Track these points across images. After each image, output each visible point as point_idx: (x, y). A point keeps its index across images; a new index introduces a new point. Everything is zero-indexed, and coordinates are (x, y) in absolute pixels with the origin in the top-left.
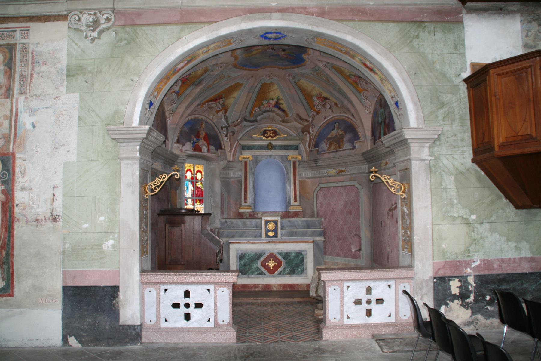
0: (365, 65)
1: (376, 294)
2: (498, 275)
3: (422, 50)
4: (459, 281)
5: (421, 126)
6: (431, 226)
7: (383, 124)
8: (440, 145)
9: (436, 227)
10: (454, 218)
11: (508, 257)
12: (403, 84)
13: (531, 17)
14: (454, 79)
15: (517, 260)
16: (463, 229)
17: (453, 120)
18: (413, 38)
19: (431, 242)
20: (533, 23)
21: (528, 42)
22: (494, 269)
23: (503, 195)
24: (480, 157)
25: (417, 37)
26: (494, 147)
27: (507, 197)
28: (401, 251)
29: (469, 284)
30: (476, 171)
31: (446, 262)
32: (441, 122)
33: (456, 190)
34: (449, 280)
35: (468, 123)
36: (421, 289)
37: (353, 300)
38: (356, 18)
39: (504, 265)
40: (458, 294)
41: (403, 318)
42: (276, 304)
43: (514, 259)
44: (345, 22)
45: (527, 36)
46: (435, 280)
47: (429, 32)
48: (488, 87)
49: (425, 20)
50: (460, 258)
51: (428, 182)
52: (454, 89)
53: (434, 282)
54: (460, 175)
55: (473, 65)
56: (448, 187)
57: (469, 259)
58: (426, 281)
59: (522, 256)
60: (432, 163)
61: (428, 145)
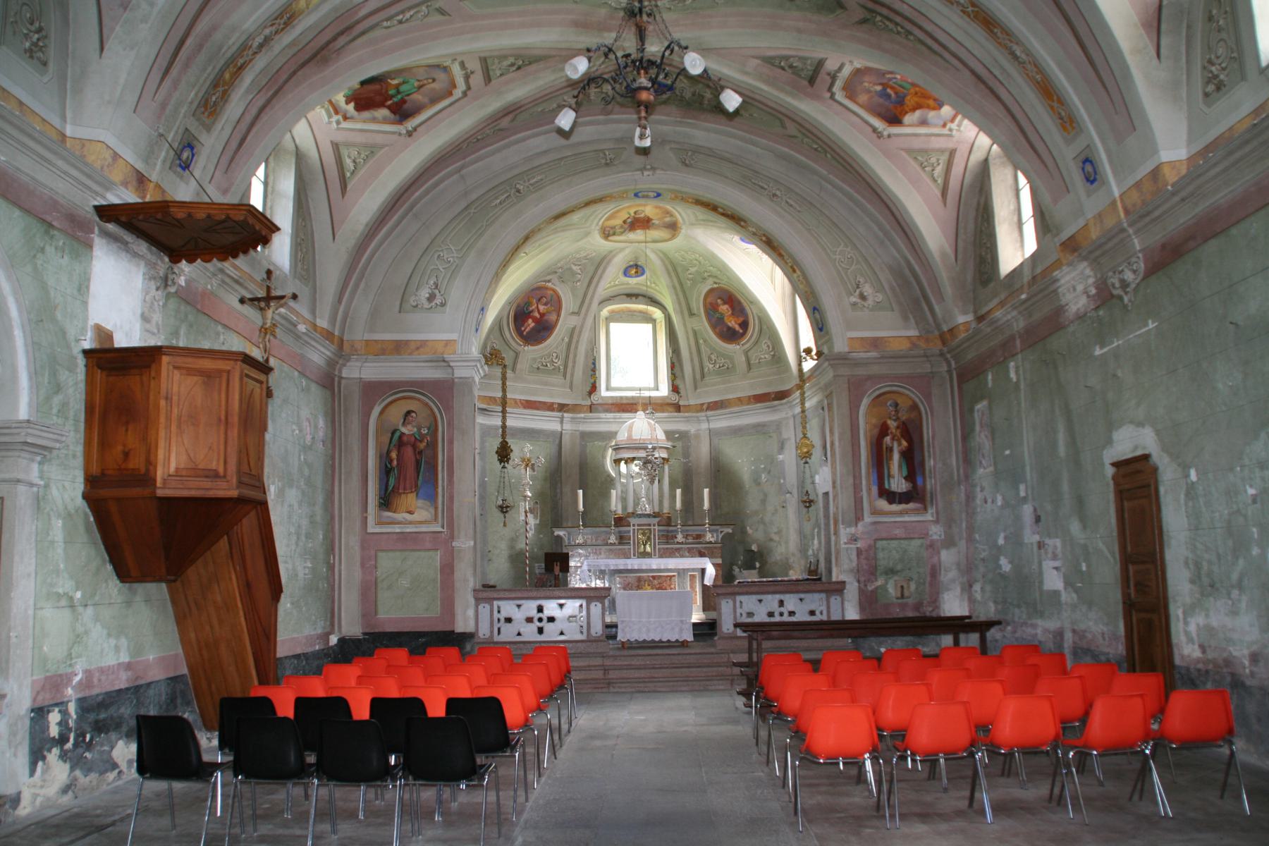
9: (39, 612)
11: (107, 664)
12: (21, 334)
15: (116, 667)
16: (67, 613)
20: (153, 282)
23: (107, 558)
26: (155, 480)
30: (86, 514)
40: (57, 737)
43: (113, 666)
45: (145, 301)
46: (32, 715)
47: (56, 248)
49: (55, 223)
51: (34, 527)
53: (32, 719)
54: (68, 517)
57: (70, 670)
61: (39, 458)
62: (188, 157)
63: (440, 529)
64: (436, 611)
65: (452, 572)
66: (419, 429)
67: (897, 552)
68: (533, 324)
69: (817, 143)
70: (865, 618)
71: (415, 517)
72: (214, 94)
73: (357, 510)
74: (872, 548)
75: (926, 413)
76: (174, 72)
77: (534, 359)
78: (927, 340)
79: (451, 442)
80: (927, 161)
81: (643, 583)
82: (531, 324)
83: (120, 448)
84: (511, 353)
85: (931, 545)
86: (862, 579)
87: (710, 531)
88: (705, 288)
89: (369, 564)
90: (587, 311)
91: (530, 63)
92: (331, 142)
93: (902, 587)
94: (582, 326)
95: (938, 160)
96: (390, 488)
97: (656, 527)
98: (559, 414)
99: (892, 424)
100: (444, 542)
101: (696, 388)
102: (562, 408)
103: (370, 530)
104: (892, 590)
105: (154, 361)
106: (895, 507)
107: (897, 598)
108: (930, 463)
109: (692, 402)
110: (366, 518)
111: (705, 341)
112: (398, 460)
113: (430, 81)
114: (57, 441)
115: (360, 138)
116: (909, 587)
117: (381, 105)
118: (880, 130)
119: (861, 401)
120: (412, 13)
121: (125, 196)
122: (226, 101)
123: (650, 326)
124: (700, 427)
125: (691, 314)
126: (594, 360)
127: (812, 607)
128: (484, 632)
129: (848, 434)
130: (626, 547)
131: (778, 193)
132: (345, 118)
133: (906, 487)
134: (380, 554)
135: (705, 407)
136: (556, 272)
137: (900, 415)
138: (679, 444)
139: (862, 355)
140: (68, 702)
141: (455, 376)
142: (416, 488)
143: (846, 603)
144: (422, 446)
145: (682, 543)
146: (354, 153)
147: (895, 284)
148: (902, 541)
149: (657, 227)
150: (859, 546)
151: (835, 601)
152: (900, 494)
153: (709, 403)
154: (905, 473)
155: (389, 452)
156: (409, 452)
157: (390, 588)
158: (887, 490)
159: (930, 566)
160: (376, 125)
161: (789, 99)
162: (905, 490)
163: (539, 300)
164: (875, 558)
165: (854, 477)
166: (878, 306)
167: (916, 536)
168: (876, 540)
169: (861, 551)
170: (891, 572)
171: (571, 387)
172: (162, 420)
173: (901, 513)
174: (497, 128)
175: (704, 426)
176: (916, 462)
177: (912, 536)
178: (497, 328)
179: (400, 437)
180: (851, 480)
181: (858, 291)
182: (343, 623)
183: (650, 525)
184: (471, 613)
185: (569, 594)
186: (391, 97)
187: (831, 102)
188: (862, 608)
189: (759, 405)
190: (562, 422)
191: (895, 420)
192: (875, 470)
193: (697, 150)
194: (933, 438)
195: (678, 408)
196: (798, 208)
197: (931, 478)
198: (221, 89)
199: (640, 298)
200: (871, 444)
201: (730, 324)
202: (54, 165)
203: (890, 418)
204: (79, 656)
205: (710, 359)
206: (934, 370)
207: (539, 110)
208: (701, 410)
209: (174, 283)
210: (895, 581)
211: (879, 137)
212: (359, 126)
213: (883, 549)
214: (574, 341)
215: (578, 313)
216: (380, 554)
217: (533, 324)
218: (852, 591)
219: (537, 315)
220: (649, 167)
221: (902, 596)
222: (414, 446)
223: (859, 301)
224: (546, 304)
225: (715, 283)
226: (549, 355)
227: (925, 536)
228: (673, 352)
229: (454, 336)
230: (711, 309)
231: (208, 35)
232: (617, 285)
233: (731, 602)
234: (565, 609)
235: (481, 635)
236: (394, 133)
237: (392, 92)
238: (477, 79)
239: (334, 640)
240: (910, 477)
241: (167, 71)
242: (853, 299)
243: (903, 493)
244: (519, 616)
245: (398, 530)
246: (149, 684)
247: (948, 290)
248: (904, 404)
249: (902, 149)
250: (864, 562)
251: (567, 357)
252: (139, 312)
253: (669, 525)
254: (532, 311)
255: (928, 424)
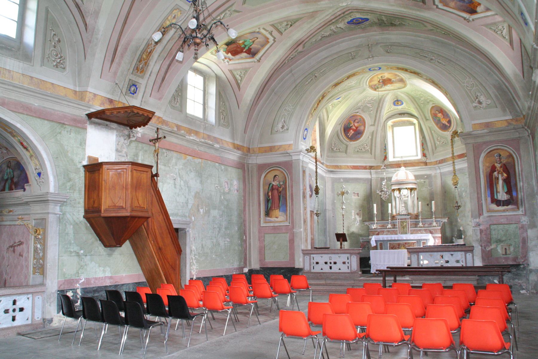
0: (22, 144)
1: (19, 305)
2: (93, 287)
3: (62, 142)
4: (72, 292)
5: (56, 192)
6: (57, 257)
7: (9, 181)
8: (66, 205)
9: (61, 258)
10: (71, 252)
11: (99, 276)
12: (49, 163)
13: (121, 134)
14: (78, 164)
16: (76, 258)
17: (75, 190)
18: (58, 134)
19: (57, 267)
20: (122, 137)
21: (118, 148)
22: (91, 284)
23: (98, 239)
24: (90, 215)
25: (60, 133)
27: (101, 240)
28: (31, 275)
29: (77, 293)
30: (85, 223)
31: (65, 280)
32: (68, 190)
33: (73, 234)
34: (67, 292)
35: (83, 193)
36: (50, 299)
37: (4, 310)
38: (25, 112)
39: (96, 281)
41: (37, 319)
42: (250, 214)
43: (102, 277)
44: (17, 114)
45: (118, 144)
47: (67, 132)
48: (101, 175)
50: (74, 278)
51: (58, 228)
52: (77, 171)
53: (58, 294)
55: (89, 158)
56: (69, 232)
57: (78, 278)
58: (53, 293)
59: (106, 275)
60: (61, 216)
61: (59, 205)
62: (134, 90)
63: (288, 224)
64: (287, 259)
65: (294, 242)
66: (279, 183)
67: (503, 231)
68: (353, 132)
69: (443, 31)
70: (485, 264)
71: (279, 219)
72: (141, 64)
73: (256, 217)
74: (489, 229)
75: (518, 160)
76: (116, 60)
77: (355, 148)
78: (517, 120)
79: (292, 187)
80: (497, 28)
81: (400, 246)
82: (352, 132)
83: (92, 200)
84: (344, 146)
85: (522, 227)
86: (483, 245)
87: (435, 221)
88: (430, 107)
89: (261, 240)
90: (378, 123)
91: (295, 23)
92: (229, 70)
93: (506, 249)
94: (377, 130)
95: (503, 27)
96: (269, 208)
97: (409, 220)
98: (369, 171)
99: (498, 166)
100: (290, 230)
101: (433, 153)
102: (371, 168)
103: (262, 225)
104: (500, 250)
105: (101, 168)
106: (501, 208)
107: (503, 255)
108: (520, 184)
109: (432, 161)
110: (260, 220)
111: (434, 131)
112: (272, 196)
113: (256, 38)
114: (65, 198)
115: (239, 67)
116: (509, 249)
117: (241, 52)
118: (467, 18)
119: (481, 154)
120: (223, 15)
121: (97, 107)
122: (148, 66)
123: (413, 127)
124: (435, 172)
125: (427, 120)
126: (385, 145)
127: (458, 259)
128: (307, 268)
129: (474, 173)
130: (396, 229)
131: (433, 58)
132: (230, 60)
133: (507, 198)
134: (266, 235)
135: (438, 162)
136: (360, 108)
137: (502, 160)
138: (427, 181)
139: (479, 132)
140: (77, 289)
141: (293, 159)
142: (279, 207)
143: (475, 257)
144: (281, 189)
145: (422, 227)
146: (239, 73)
147: (497, 93)
148: (505, 225)
149: (396, 82)
150: (481, 228)
151: (469, 255)
152: (503, 201)
153: (439, 160)
154: (506, 190)
155: (268, 193)
156: (276, 192)
157: (270, 249)
158: (496, 200)
159: (521, 238)
160: (242, 60)
161: (418, 13)
162: (506, 199)
163: (354, 121)
164: (490, 234)
165: (478, 194)
166: (488, 106)
167: (513, 222)
168: (490, 225)
169: (482, 231)
170: (499, 241)
171: (375, 158)
172: (103, 188)
173: (504, 211)
174: (298, 52)
175: (438, 171)
176: (512, 184)
177: (511, 222)
178: (336, 135)
179: (272, 186)
180: (476, 195)
181: (477, 100)
182: (252, 263)
183: (406, 219)
184: (301, 260)
185: (343, 252)
186: (244, 48)
187: (438, 10)
188: (483, 259)
189: (460, 159)
190: (371, 174)
191: (499, 163)
192: (489, 189)
193: (393, 45)
194: (522, 171)
195: (426, 164)
196: (444, 64)
197: (521, 192)
198: (143, 62)
199: (406, 114)
200: (486, 176)
201: (443, 122)
202: (62, 103)
203: (496, 163)
204: (83, 273)
205: (438, 139)
206: (521, 136)
207: (314, 40)
208: (437, 164)
209: (134, 136)
210: (502, 246)
211: (468, 22)
212: (237, 62)
213: (495, 230)
214: (374, 137)
215: (374, 125)
216: (266, 235)
217: (353, 132)
218: (478, 250)
219: (354, 128)
220: (371, 56)
221: (506, 254)
222: (278, 190)
223: (478, 105)
224: (358, 123)
225: (433, 104)
226: (363, 145)
227: (518, 222)
228: (423, 138)
229: (292, 142)
230: (434, 116)
231: (128, 44)
232: (392, 110)
233: (416, 256)
234: (323, 258)
235: (306, 269)
236: (252, 62)
237: (243, 46)
238: (275, 33)
239: (246, 270)
240: (509, 192)
241: (113, 61)
242: (475, 104)
243: (505, 200)
244: (321, 262)
245: (272, 225)
246: (123, 285)
247: (520, 93)
248: (504, 155)
249: (484, 25)
250: (484, 236)
251: (371, 145)
252: (114, 149)
253: (416, 219)
254: (352, 126)
255: (518, 164)
